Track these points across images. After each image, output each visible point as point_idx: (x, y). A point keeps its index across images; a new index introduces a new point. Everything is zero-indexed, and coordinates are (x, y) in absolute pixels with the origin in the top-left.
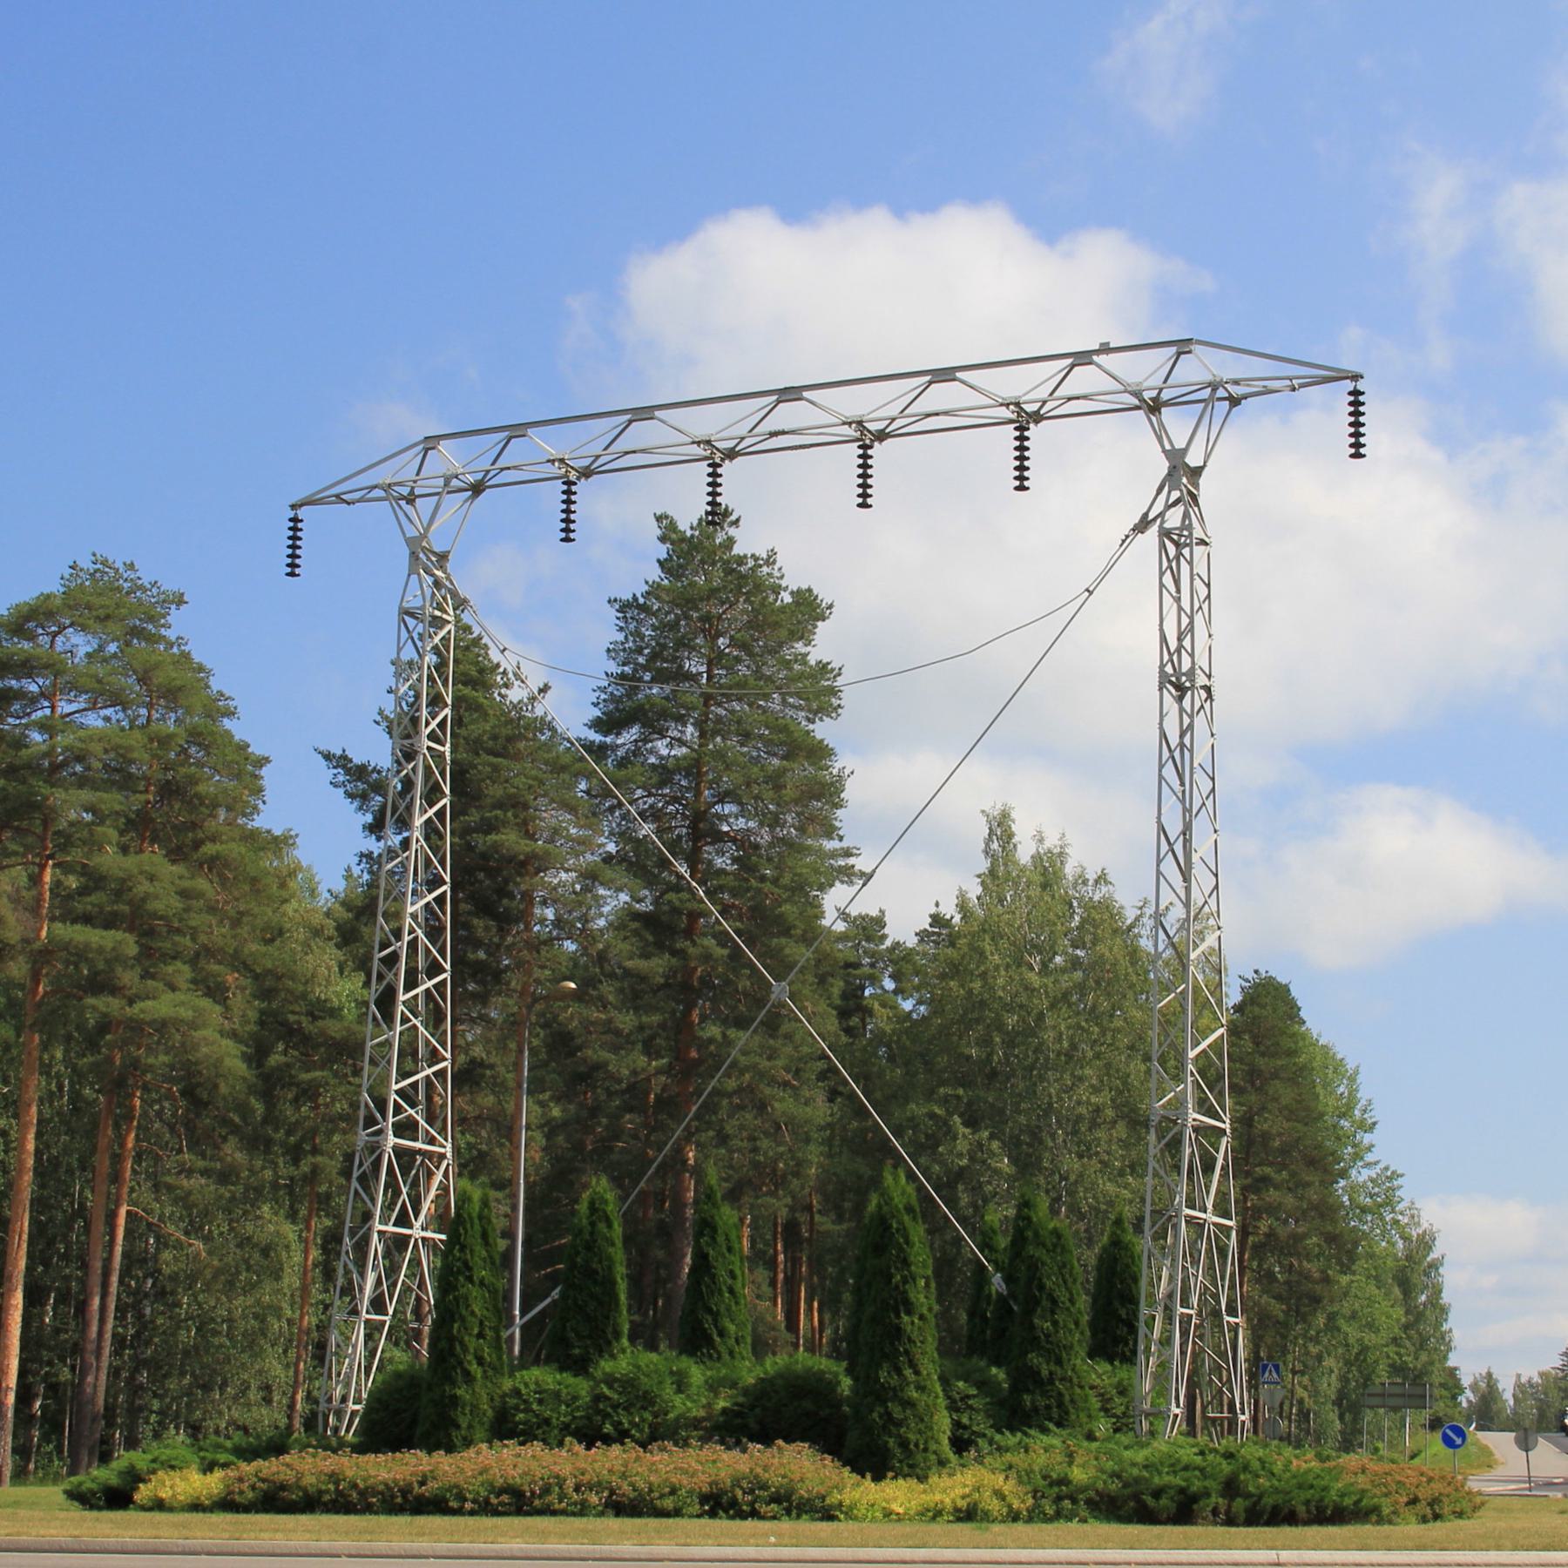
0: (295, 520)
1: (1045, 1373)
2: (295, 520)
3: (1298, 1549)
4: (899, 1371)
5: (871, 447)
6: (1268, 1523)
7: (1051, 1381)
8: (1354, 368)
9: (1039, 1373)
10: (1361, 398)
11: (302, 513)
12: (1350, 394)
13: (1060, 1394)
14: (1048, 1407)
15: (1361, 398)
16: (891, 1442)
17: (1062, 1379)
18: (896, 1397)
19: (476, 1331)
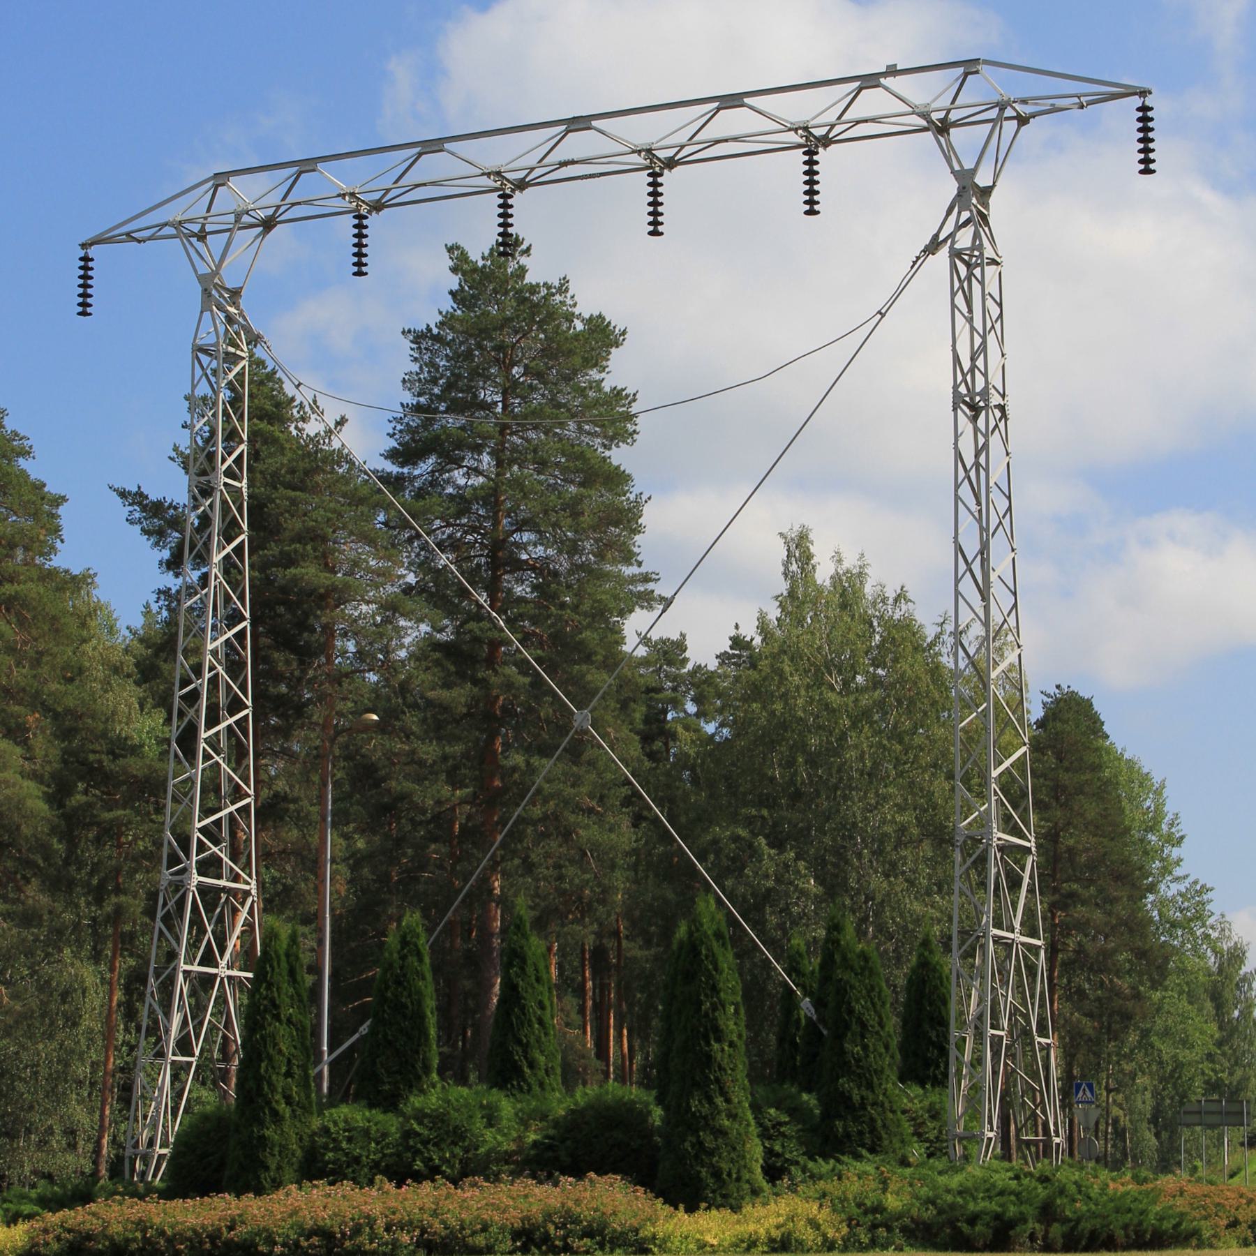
0: (86, 259)
1: (856, 1098)
4: (710, 1100)
7: (863, 1106)
9: (850, 1098)
12: (81, 259)
13: (872, 1120)
14: (861, 1133)
17: (874, 1104)
19: (284, 1069)
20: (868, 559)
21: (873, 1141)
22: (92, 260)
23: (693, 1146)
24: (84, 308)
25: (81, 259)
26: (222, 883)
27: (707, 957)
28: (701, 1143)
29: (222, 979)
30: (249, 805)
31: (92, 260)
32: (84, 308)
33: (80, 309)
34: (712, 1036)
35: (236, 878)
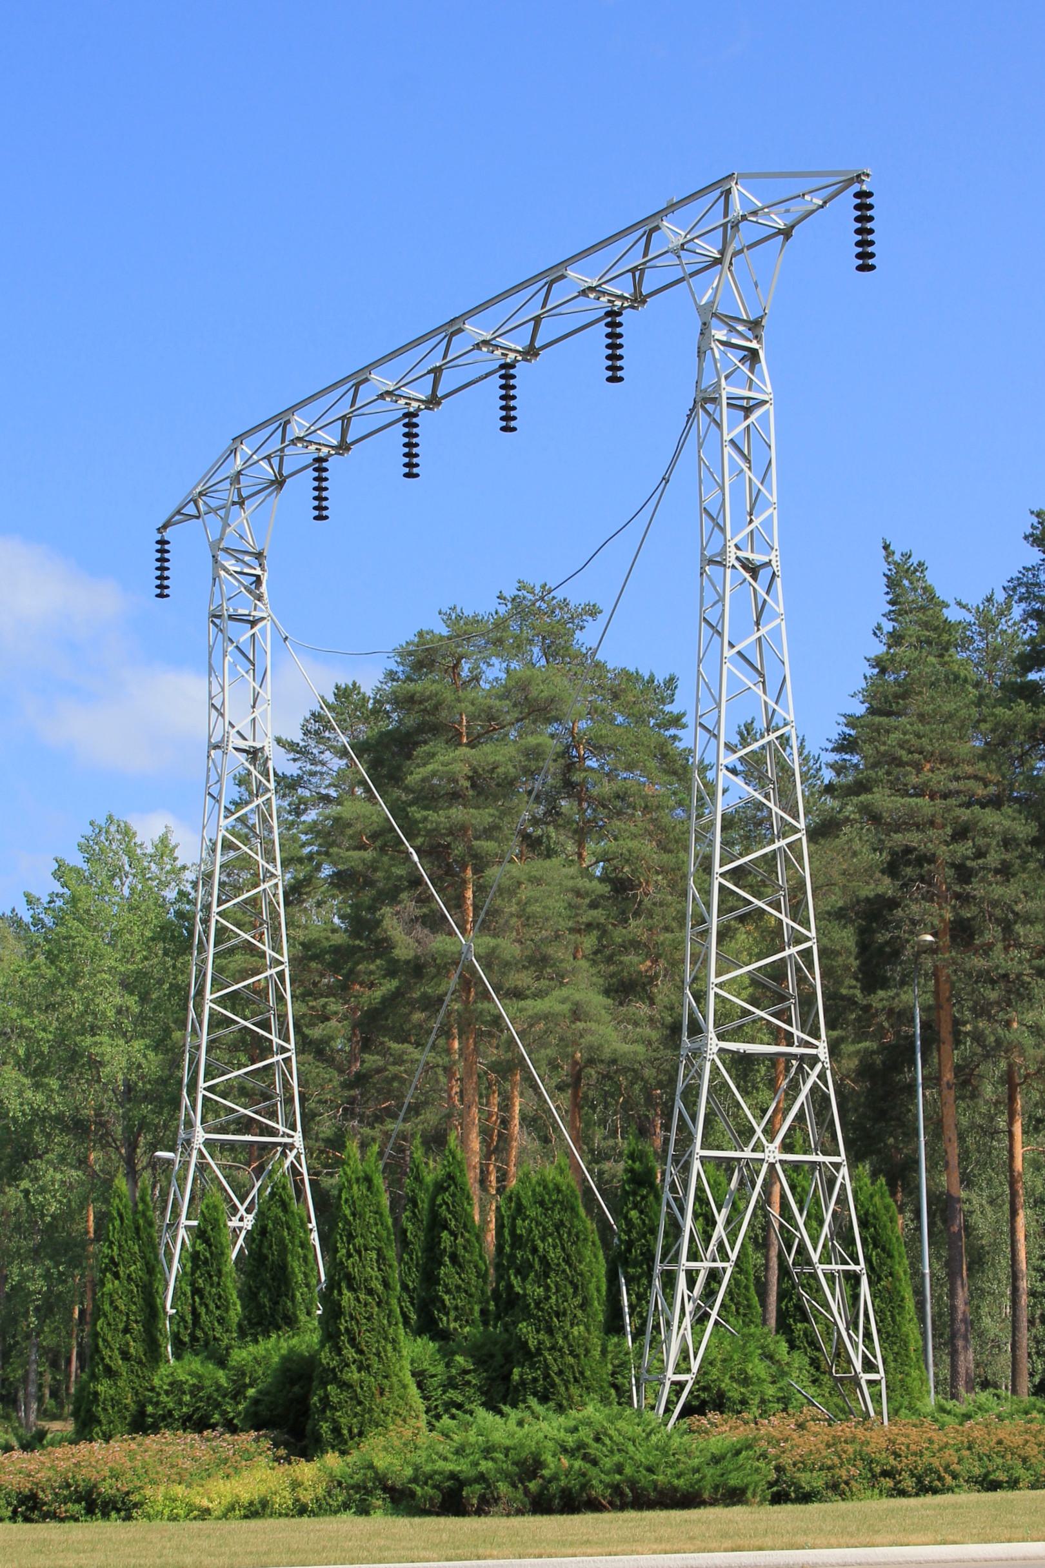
0: (162, 542)
1: (532, 1344)
2: (162, 542)
3: (1009, 1541)
4: (339, 1351)
5: (619, 314)
6: (562, 1512)
7: (539, 1351)
8: (855, 168)
9: (526, 1342)
10: (167, 547)
11: (168, 535)
12: (158, 542)
13: (547, 1367)
14: (535, 1380)
15: (167, 547)
16: (325, 1427)
17: (552, 1348)
18: (335, 1380)
19: (121, 1326)
20: (60, 856)
21: (545, 1389)
22: (168, 543)
23: (320, 1400)
24: (162, 591)
25: (158, 542)
26: (793, 1050)
27: (347, 1201)
28: (327, 1396)
29: (772, 1166)
30: (717, 976)
31: (168, 543)
32: (162, 591)
33: (158, 591)
34: (343, 1285)
35: (808, 1045)
